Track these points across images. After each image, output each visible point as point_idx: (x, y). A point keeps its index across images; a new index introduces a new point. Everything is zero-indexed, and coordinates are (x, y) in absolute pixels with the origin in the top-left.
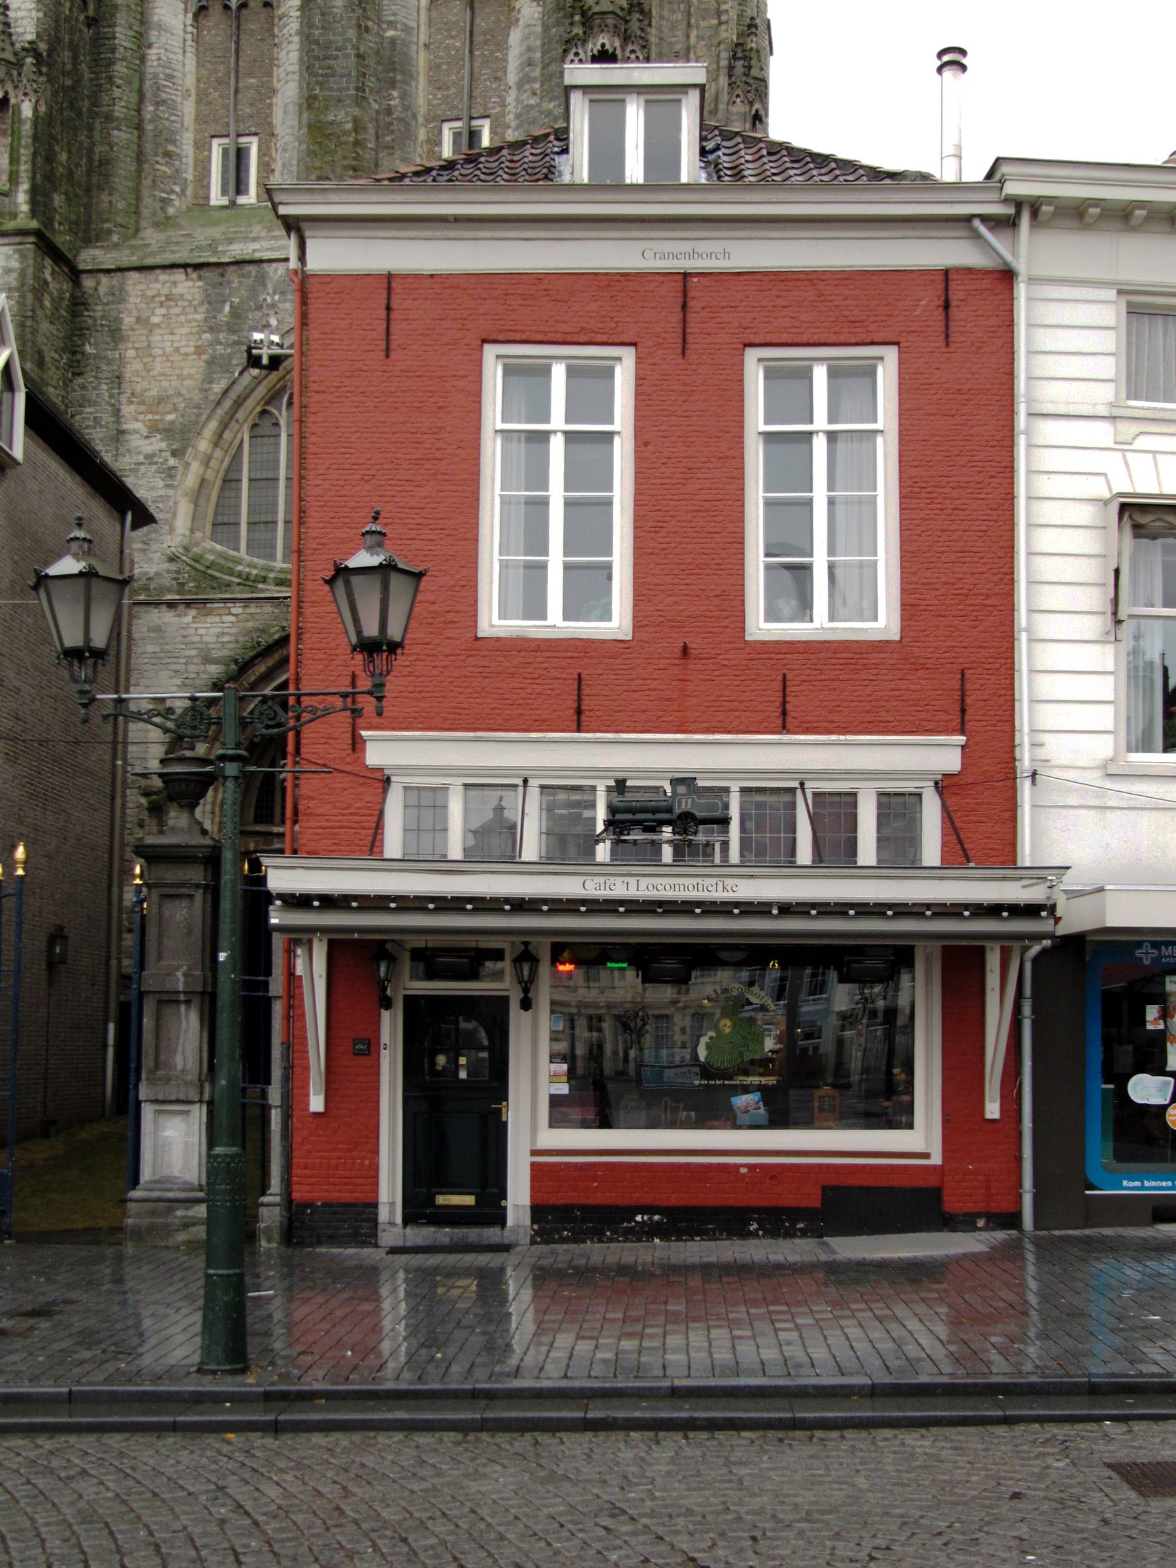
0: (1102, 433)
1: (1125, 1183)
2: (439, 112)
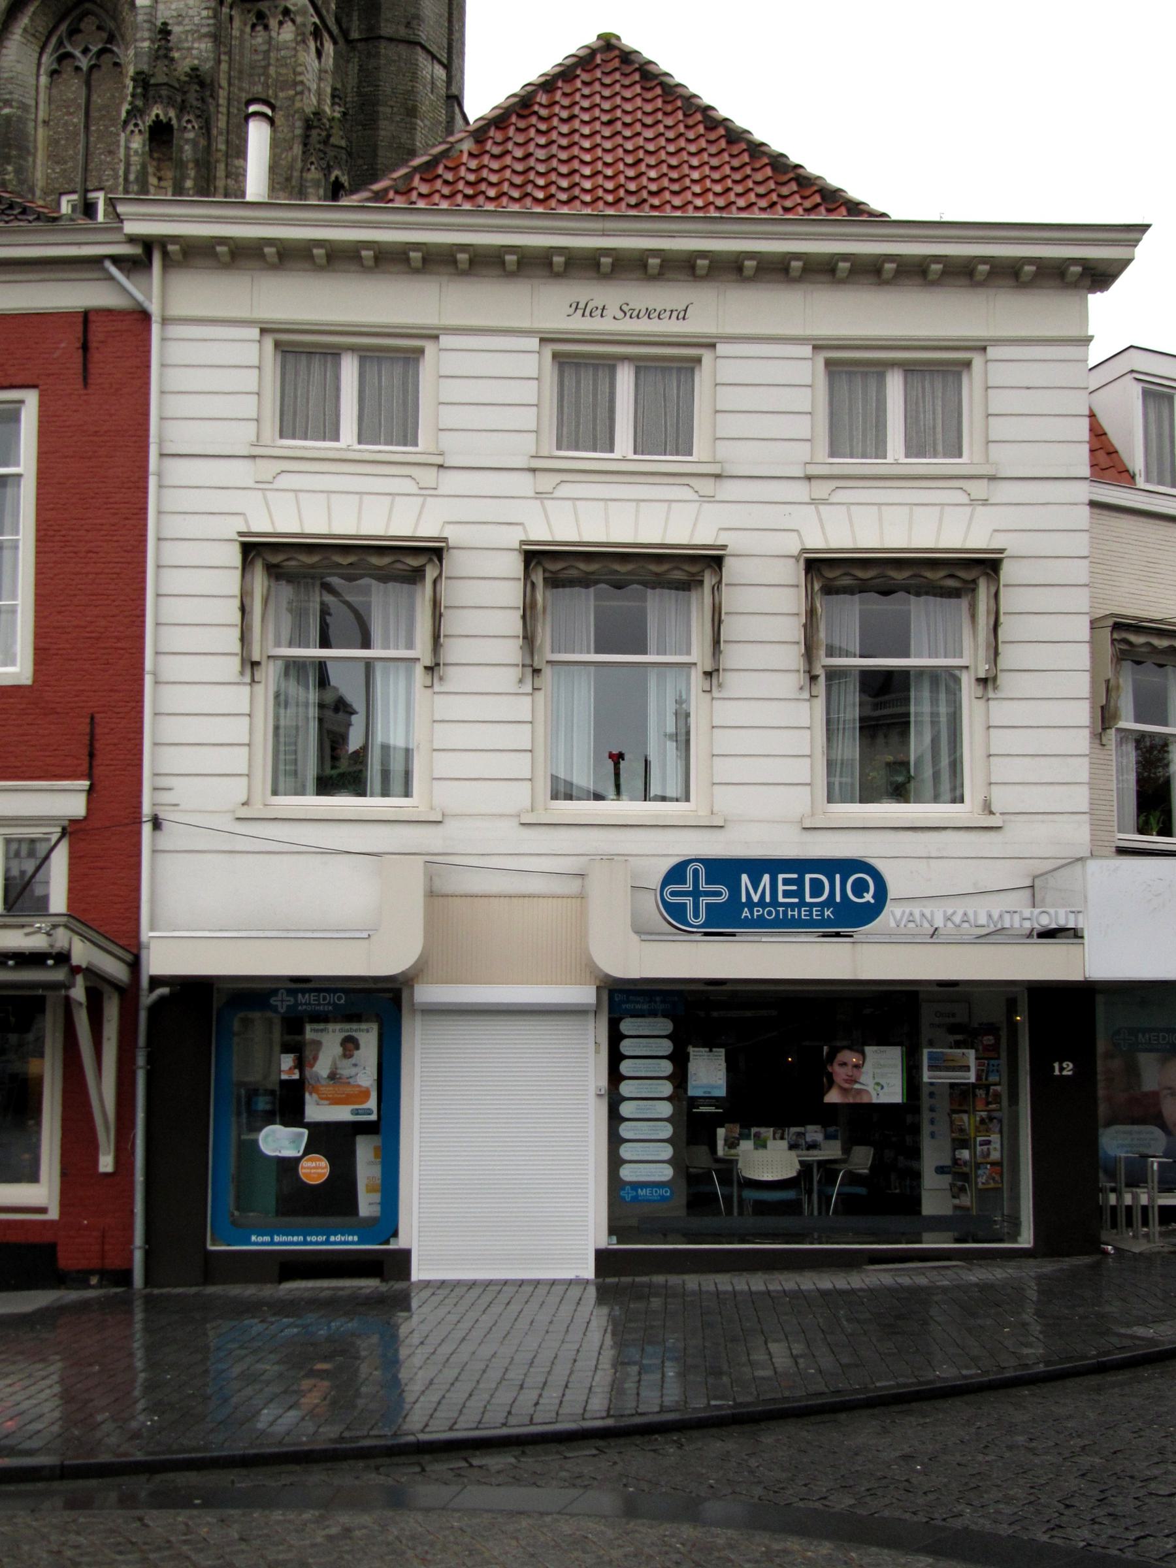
0: (524, 484)
1: (253, 1238)
2: (57, 186)
